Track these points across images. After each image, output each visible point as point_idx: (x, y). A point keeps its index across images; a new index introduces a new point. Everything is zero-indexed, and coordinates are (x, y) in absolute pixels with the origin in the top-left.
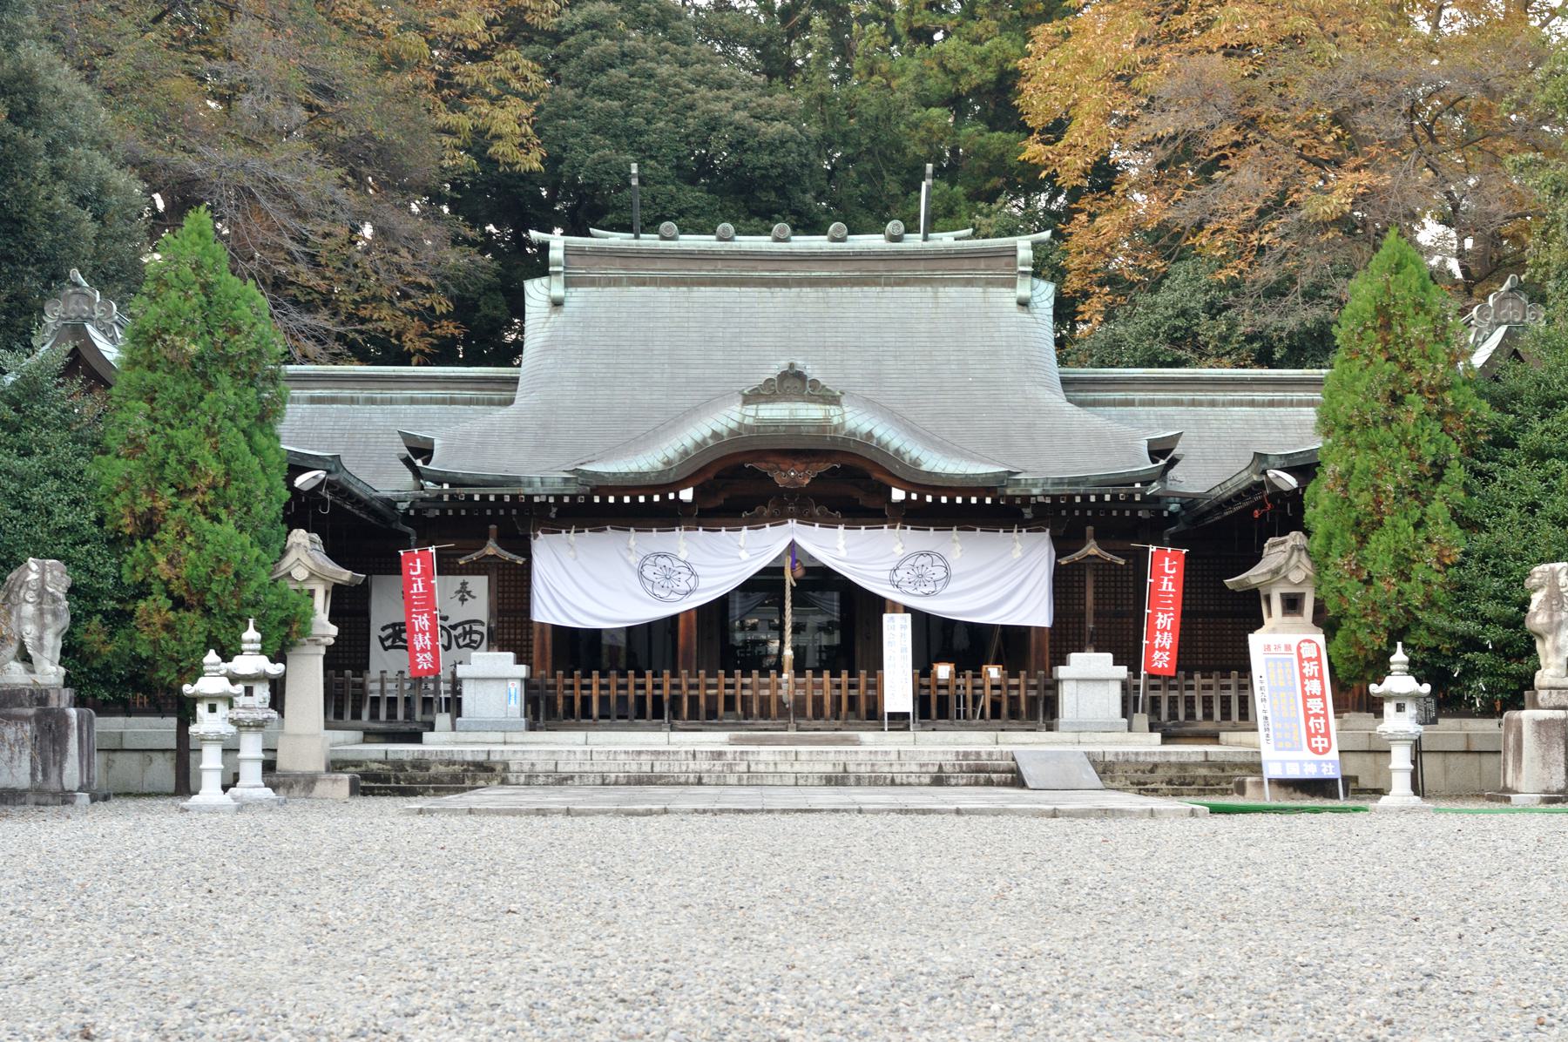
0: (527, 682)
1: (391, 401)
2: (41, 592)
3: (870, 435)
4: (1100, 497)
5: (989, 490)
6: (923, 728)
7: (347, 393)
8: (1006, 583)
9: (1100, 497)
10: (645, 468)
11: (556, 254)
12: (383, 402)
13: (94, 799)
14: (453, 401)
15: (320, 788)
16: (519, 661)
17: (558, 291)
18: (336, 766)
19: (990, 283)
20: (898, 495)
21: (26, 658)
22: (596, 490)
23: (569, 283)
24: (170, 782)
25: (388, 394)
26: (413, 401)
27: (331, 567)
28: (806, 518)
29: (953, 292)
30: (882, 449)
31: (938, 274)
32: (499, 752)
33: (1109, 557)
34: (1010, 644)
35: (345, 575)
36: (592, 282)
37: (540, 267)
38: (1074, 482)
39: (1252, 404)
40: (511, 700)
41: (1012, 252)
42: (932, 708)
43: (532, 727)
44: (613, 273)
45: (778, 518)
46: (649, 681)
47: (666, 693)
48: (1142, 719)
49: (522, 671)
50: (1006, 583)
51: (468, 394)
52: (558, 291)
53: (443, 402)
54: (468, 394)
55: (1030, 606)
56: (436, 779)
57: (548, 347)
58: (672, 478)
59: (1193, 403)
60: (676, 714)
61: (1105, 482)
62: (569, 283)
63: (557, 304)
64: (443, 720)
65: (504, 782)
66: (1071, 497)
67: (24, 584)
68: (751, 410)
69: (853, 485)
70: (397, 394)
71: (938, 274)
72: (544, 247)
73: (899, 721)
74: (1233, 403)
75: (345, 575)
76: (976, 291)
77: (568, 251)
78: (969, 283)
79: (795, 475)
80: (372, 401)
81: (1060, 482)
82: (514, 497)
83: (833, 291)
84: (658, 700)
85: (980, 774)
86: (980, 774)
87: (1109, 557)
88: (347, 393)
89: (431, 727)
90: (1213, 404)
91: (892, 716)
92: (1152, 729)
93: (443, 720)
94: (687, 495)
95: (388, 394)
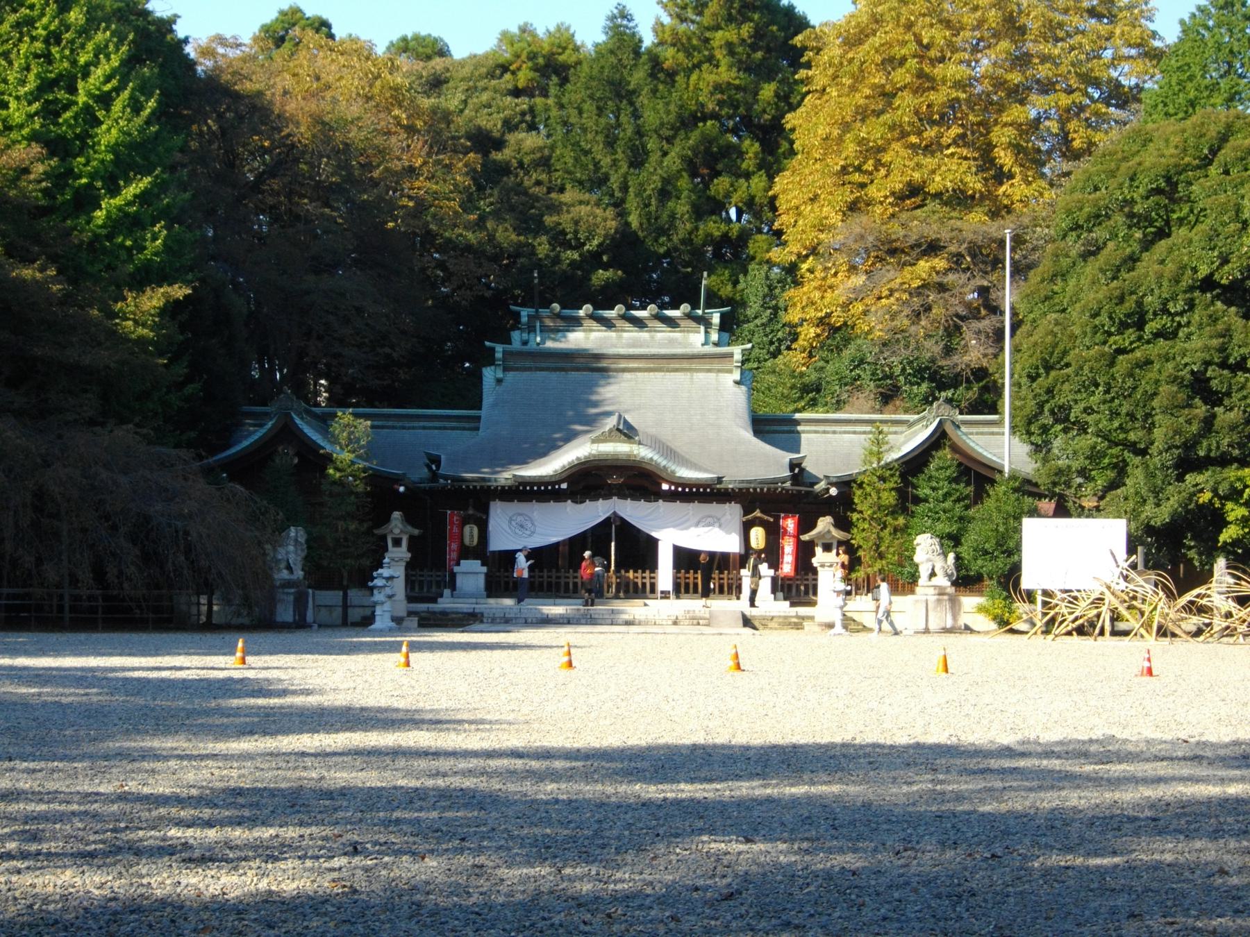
0: (487, 575)
1: (414, 428)
2: (296, 540)
3: (651, 459)
4: (762, 489)
5: (709, 486)
6: (678, 597)
7: (390, 423)
8: (716, 535)
9: (762, 489)
10: (544, 474)
11: (499, 355)
12: (409, 428)
13: (320, 626)
14: (445, 428)
15: (405, 624)
16: (483, 565)
17: (500, 375)
18: (410, 614)
19: (719, 371)
20: (665, 487)
21: (289, 568)
22: (520, 484)
23: (505, 369)
24: (339, 621)
25: (412, 424)
26: (424, 428)
27: (409, 528)
28: (623, 496)
29: (701, 375)
30: (657, 465)
31: (693, 366)
32: (479, 608)
33: (766, 517)
34: (720, 562)
35: (416, 532)
36: (517, 369)
37: (489, 359)
38: (749, 482)
39: (855, 433)
40: (481, 581)
41: (731, 355)
42: (681, 589)
43: (489, 596)
44: (528, 364)
45: (607, 496)
46: (545, 574)
47: (554, 580)
48: (780, 595)
49: (484, 569)
50: (716, 535)
51: (454, 424)
52: (500, 375)
53: (440, 428)
54: (454, 424)
55: (729, 543)
56: (453, 620)
57: (494, 405)
58: (557, 478)
59: (824, 432)
60: (558, 590)
61: (763, 482)
62: (505, 369)
63: (499, 381)
64: (447, 592)
65: (482, 622)
66: (748, 489)
67: (288, 536)
68: (595, 446)
69: (641, 482)
70: (416, 424)
71: (693, 366)
72: (493, 350)
73: (665, 595)
74: (845, 432)
75: (416, 532)
76: (712, 375)
77: (504, 352)
78: (709, 371)
79: (614, 480)
80: (404, 428)
81: (743, 481)
82: (482, 487)
83: (639, 374)
84: (550, 584)
85: (696, 621)
86: (696, 621)
87: (766, 517)
88: (390, 423)
89: (441, 596)
90: (834, 432)
91: (662, 592)
92: (785, 599)
93: (447, 592)
94: (564, 486)
95: (412, 424)
